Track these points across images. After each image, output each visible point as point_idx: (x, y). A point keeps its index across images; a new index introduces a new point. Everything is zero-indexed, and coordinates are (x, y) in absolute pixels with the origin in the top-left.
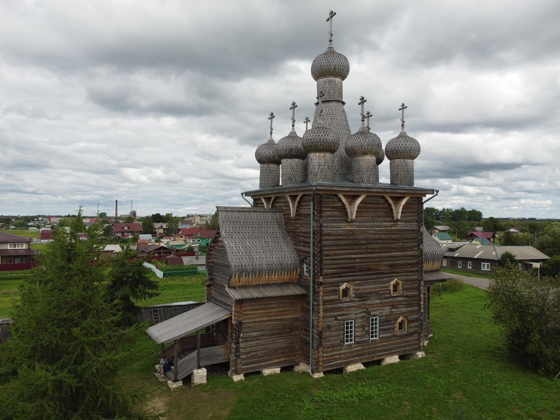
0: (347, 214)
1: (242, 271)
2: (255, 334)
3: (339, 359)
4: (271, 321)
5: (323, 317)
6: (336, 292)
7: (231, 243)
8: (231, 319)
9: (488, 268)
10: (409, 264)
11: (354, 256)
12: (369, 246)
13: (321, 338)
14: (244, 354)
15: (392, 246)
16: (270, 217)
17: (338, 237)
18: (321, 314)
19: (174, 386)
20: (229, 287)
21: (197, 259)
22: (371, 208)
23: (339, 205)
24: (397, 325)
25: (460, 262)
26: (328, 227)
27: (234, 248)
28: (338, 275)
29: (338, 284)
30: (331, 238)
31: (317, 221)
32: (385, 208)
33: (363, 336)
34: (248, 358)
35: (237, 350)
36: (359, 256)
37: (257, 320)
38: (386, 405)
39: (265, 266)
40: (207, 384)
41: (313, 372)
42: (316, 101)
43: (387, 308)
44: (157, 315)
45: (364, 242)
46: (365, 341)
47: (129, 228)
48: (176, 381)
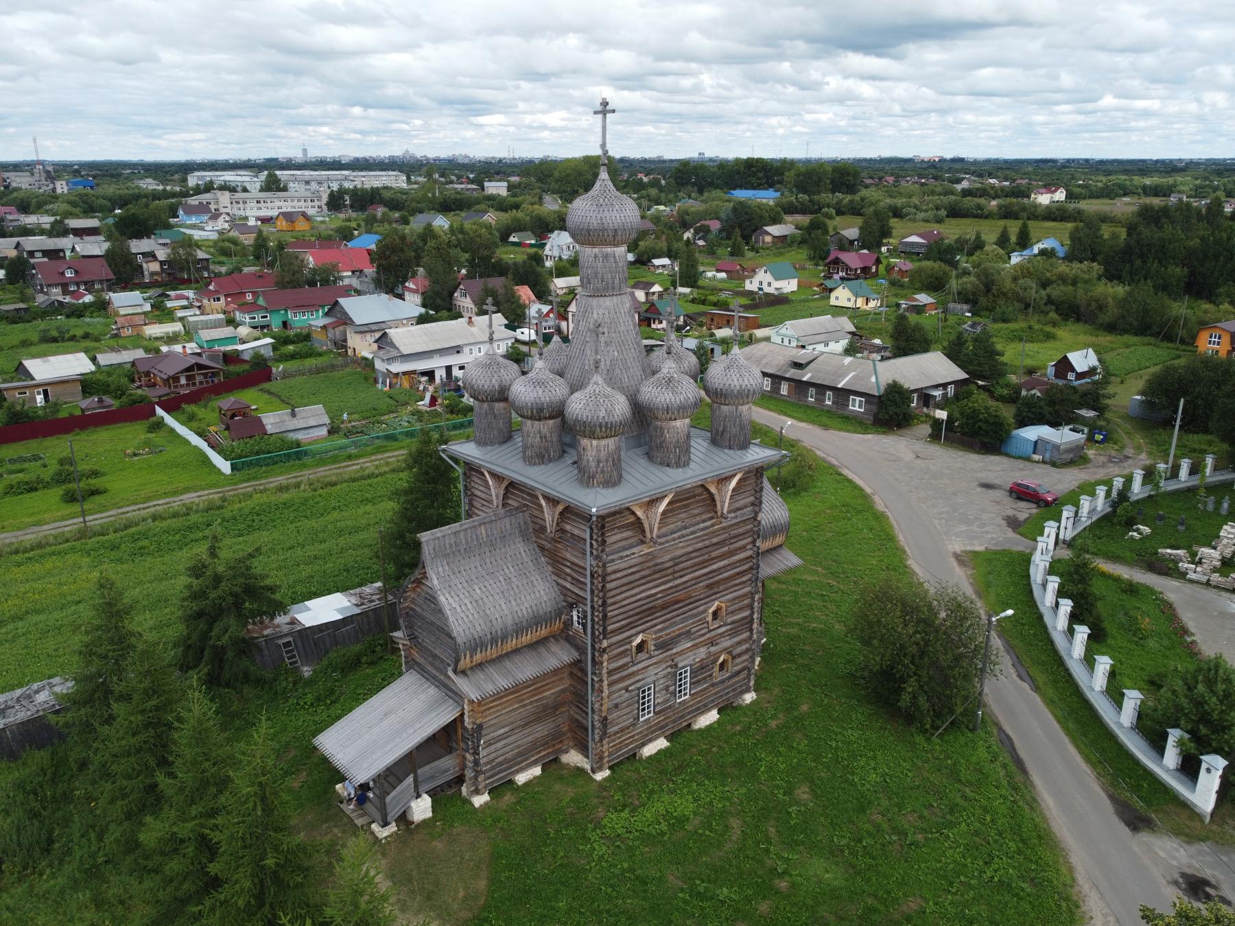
0: (643, 531)
1: (477, 645)
2: (502, 731)
3: (631, 743)
5: (610, 694)
7: (451, 601)
8: (463, 721)
9: (860, 406)
10: (738, 574)
11: (653, 591)
12: (676, 568)
14: (486, 764)
15: (713, 555)
16: (508, 527)
17: (630, 571)
18: (606, 692)
19: (385, 834)
20: (455, 671)
21: (293, 415)
22: (680, 508)
23: (632, 519)
24: (717, 668)
25: (812, 391)
27: (459, 609)
28: (629, 626)
29: (629, 640)
30: (619, 575)
31: (597, 558)
32: (704, 500)
33: (667, 701)
34: (493, 768)
35: (476, 763)
36: (662, 588)
38: (707, 833)
39: (509, 622)
40: (434, 819)
41: (594, 772)
43: (702, 649)
44: (292, 651)
45: (671, 563)
46: (670, 707)
47: (76, 272)
48: (385, 824)
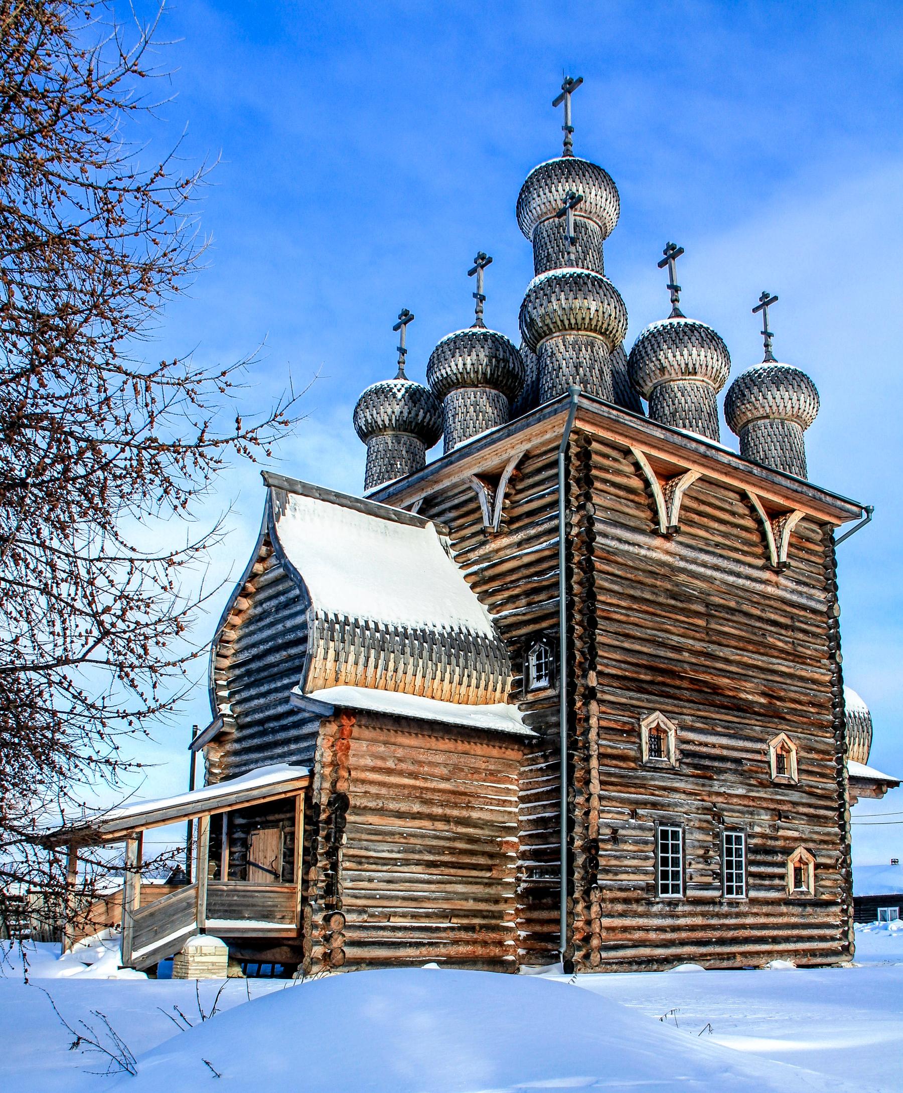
4: (432, 818)
6: (634, 732)
13: (592, 862)
26: (482, 927)
29: (636, 712)
37: (392, 806)
42: (386, 731)
